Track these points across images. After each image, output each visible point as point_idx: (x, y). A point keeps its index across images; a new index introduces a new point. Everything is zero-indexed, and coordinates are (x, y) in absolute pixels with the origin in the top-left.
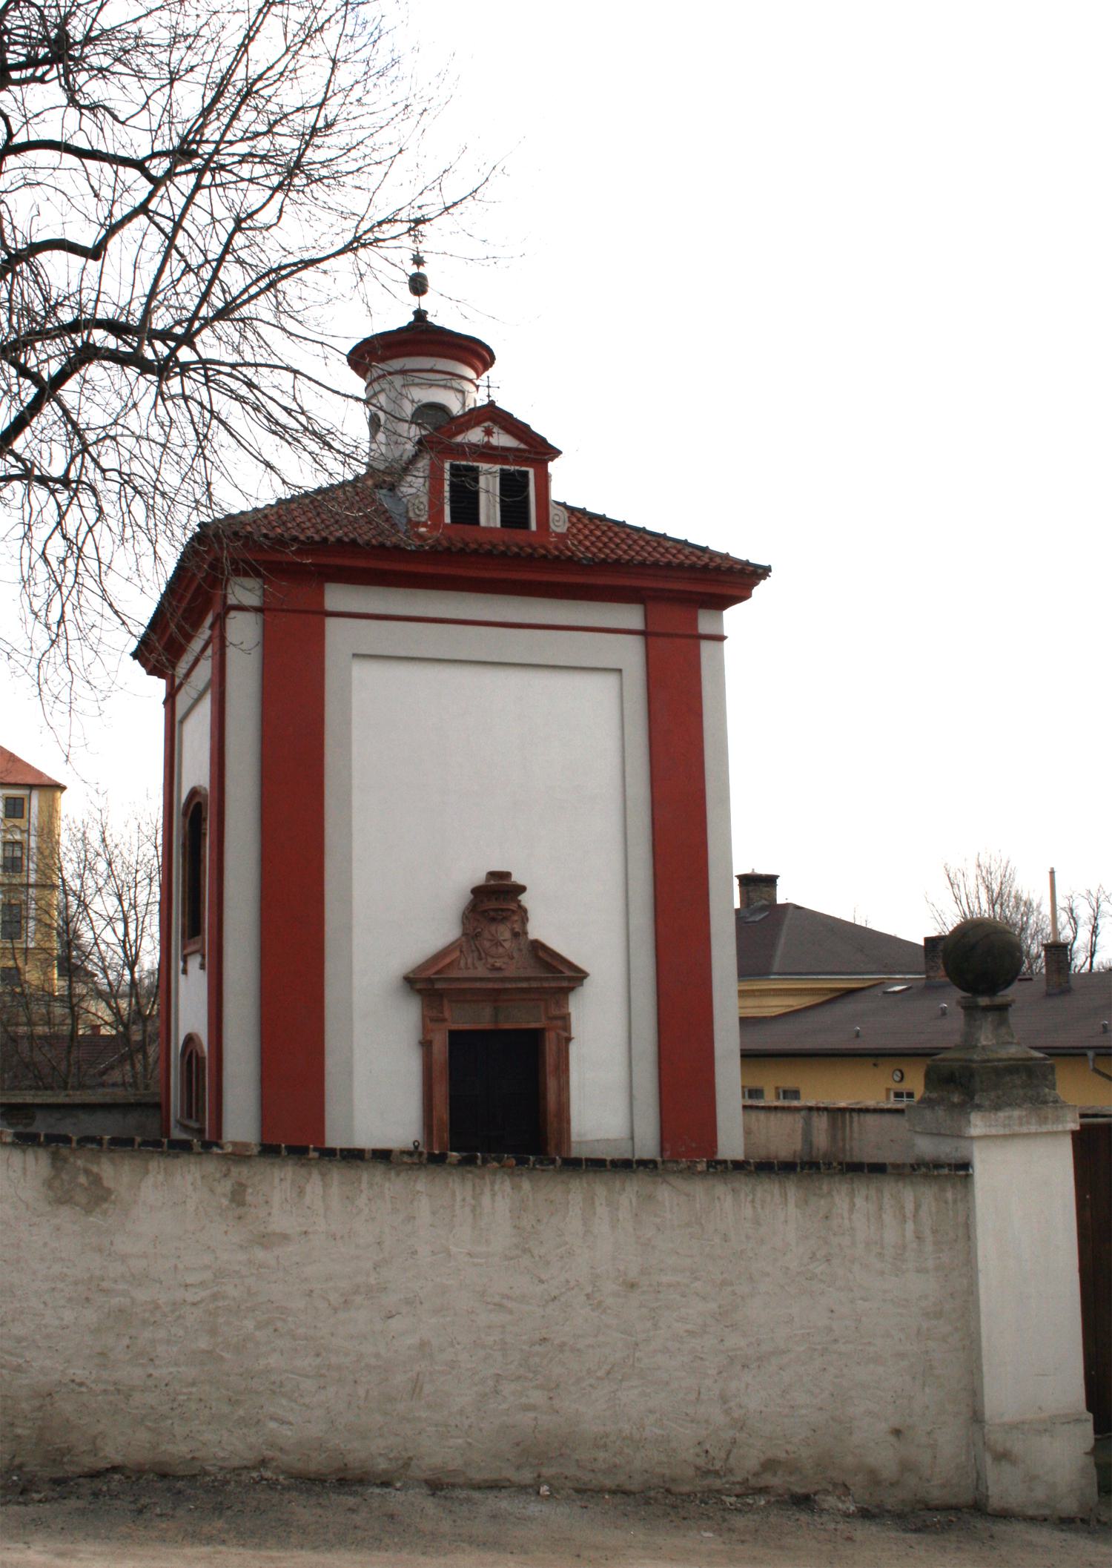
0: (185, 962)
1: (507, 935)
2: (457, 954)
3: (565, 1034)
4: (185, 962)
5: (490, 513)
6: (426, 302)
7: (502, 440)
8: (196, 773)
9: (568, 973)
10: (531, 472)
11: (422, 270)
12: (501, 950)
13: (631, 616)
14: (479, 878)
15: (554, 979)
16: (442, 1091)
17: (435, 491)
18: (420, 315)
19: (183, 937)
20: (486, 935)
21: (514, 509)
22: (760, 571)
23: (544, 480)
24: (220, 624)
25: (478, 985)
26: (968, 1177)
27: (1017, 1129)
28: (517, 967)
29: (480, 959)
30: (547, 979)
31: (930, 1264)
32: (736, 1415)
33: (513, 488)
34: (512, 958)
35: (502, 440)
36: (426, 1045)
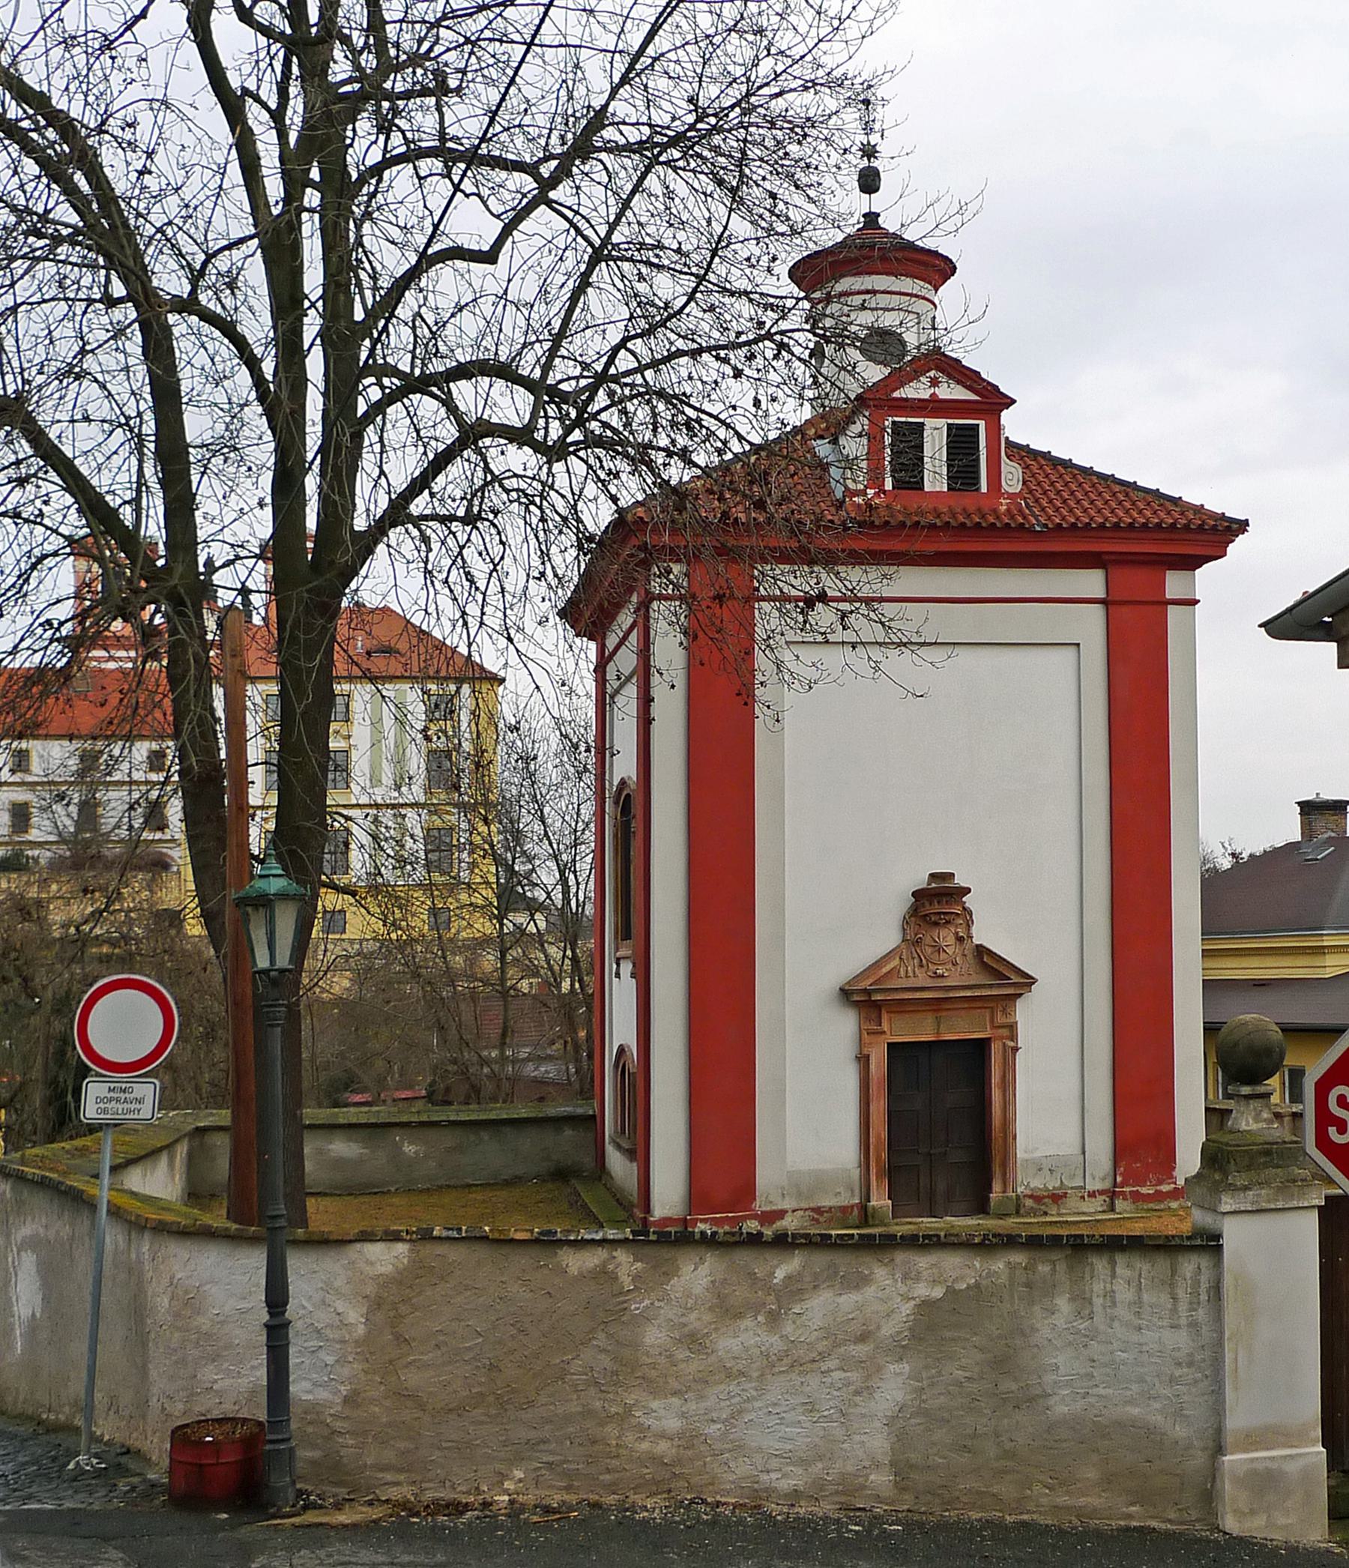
0: (618, 965)
1: (951, 940)
2: (896, 962)
3: (1012, 1044)
4: (618, 965)
5: (935, 478)
6: (877, 202)
7: (950, 391)
8: (624, 767)
9: (1015, 979)
10: (982, 424)
11: (875, 163)
12: (943, 955)
13: (1091, 582)
14: (921, 881)
15: (999, 986)
16: (879, 1108)
17: (874, 455)
18: (871, 219)
19: (616, 938)
20: (928, 940)
21: (962, 473)
22: (1235, 526)
23: (995, 429)
24: (644, 607)
25: (918, 995)
26: (1219, 1248)
27: (1265, 1205)
28: (959, 975)
29: (921, 966)
30: (991, 986)
31: (1183, 1321)
32: (1007, 1448)
33: (961, 443)
34: (955, 964)
35: (950, 391)
36: (863, 1060)
